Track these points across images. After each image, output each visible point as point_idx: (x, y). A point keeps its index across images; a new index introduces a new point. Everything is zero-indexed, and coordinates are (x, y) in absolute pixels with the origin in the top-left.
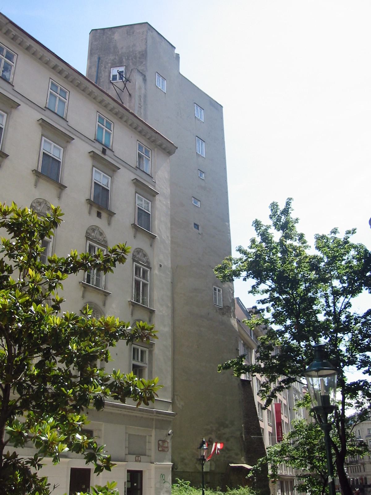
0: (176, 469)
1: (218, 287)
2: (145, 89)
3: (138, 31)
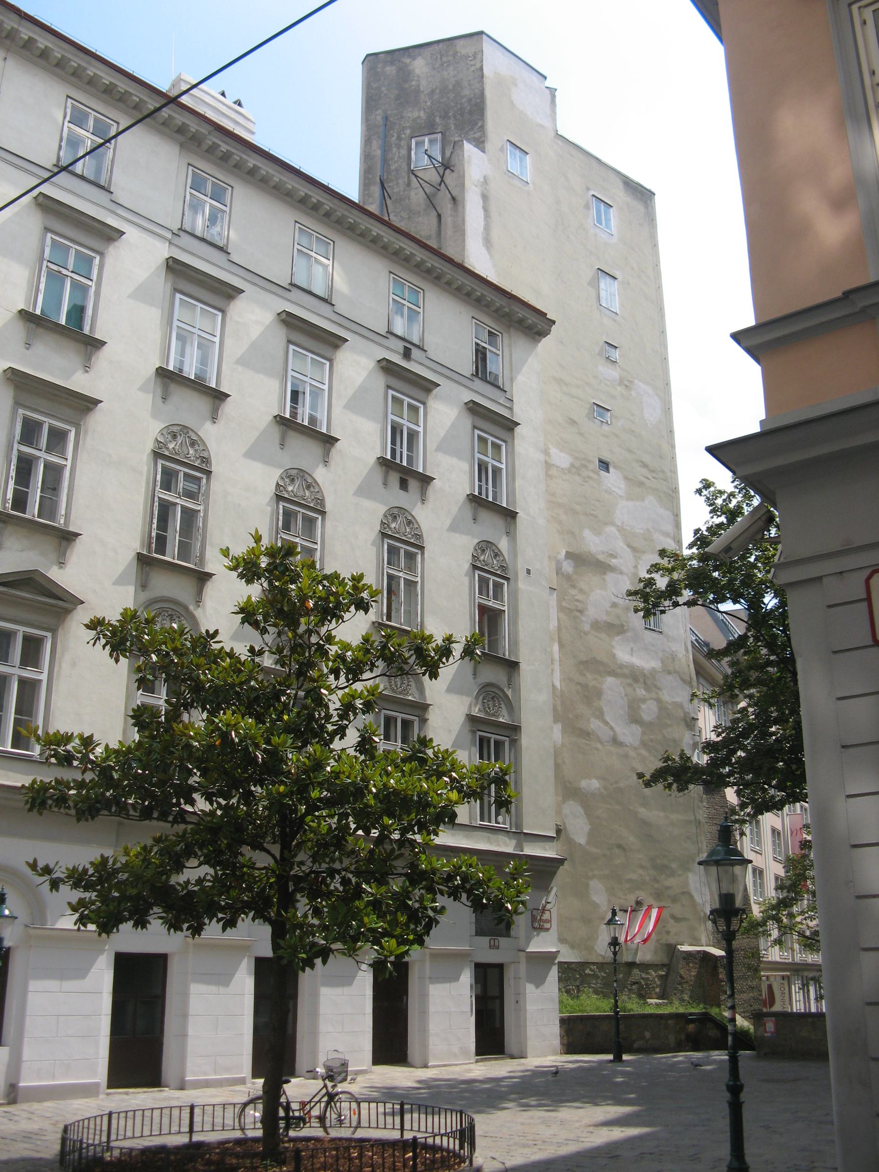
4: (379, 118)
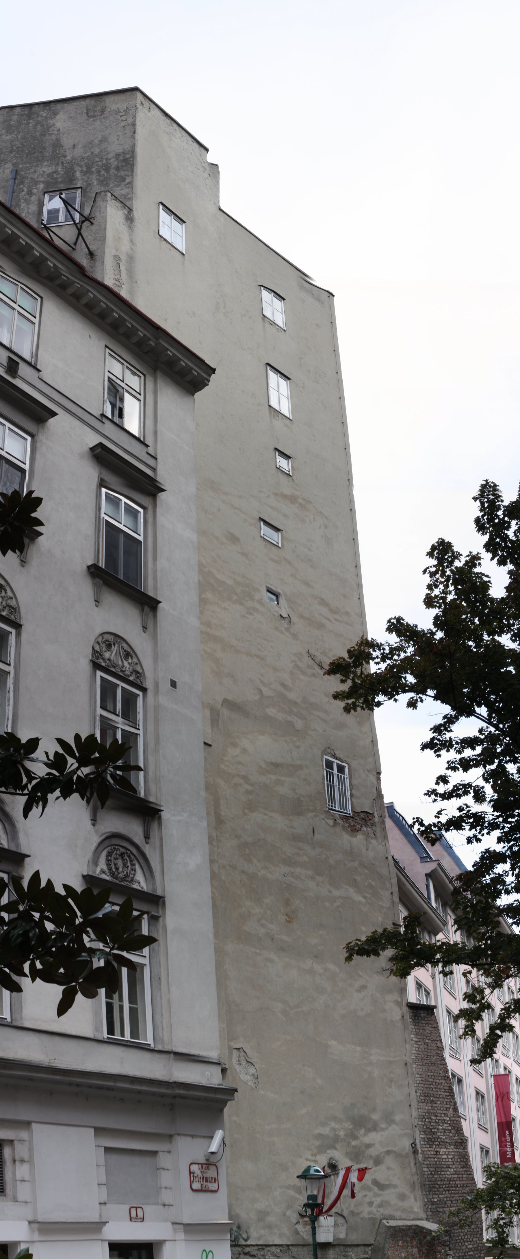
0: (246, 1240)
1: (337, 759)
2: (132, 241)
3: (114, 107)
4: (8, 171)
